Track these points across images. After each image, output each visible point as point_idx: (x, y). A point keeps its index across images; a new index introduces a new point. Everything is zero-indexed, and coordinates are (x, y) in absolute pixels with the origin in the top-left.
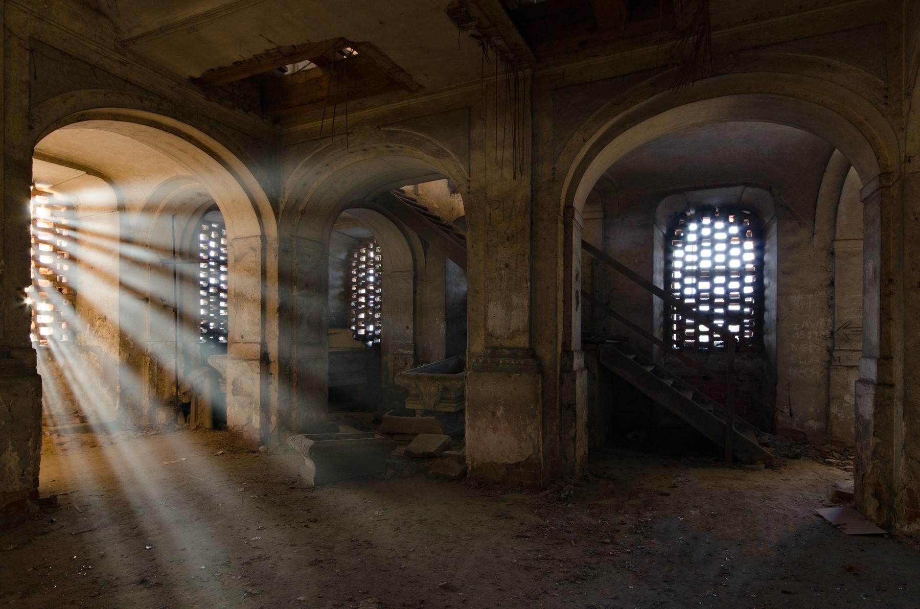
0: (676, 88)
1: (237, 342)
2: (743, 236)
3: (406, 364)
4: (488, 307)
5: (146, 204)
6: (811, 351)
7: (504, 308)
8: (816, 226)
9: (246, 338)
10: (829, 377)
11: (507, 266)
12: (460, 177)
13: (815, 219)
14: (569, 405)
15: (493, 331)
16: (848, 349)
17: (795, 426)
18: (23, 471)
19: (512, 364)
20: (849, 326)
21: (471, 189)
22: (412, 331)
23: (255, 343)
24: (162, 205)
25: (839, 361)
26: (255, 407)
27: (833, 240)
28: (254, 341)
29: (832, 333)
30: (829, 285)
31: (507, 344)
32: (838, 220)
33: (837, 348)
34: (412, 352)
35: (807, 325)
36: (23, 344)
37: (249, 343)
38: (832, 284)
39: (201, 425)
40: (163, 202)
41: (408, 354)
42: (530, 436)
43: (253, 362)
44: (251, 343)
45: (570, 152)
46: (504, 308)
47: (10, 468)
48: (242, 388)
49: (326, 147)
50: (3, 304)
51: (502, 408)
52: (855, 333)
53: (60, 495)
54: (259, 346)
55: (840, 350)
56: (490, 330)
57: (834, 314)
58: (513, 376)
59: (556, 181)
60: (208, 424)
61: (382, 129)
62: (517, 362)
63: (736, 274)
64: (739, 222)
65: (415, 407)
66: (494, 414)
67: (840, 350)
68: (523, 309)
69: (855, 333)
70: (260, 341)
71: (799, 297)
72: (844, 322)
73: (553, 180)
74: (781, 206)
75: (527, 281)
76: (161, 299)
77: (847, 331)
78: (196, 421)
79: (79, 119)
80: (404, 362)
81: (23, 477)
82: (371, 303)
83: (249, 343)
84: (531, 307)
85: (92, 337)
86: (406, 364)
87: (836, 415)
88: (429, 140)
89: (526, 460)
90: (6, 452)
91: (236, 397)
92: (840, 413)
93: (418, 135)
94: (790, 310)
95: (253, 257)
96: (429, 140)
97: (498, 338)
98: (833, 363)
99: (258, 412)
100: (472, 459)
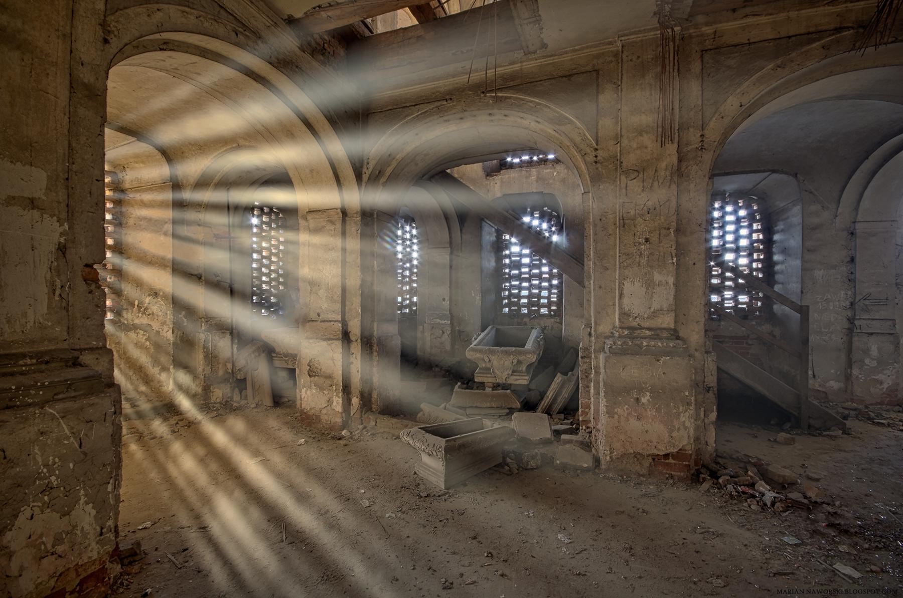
0: (863, 50)
1: (313, 321)
2: (751, 218)
3: (443, 333)
4: (623, 284)
5: (202, 176)
6: (832, 319)
7: (644, 285)
8: (839, 208)
9: (323, 316)
10: (850, 342)
11: (647, 240)
12: (586, 145)
13: (839, 203)
14: (710, 387)
15: (629, 310)
16: (867, 317)
17: (817, 386)
18: (102, 529)
19: (659, 347)
20: (869, 298)
21: (599, 158)
22: (448, 302)
23: (335, 321)
24: (217, 178)
25: (860, 329)
26: (336, 390)
27: (854, 222)
28: (334, 320)
29: (852, 304)
30: (849, 261)
31: (646, 324)
32: (861, 203)
33: (857, 317)
34: (449, 322)
35: (829, 297)
36: (95, 343)
37: (327, 321)
38: (852, 260)
39: (260, 403)
40: (218, 175)
41: (445, 324)
42: (684, 425)
43: (334, 341)
44: (331, 321)
45: (722, 118)
46: (644, 285)
47: (83, 528)
48: (321, 370)
49: (419, 115)
50: (67, 289)
51: (648, 394)
52: (873, 304)
53: (139, 529)
54: (340, 325)
55: (860, 319)
56: (626, 309)
57: (855, 287)
58: (662, 359)
59: (705, 149)
60: (268, 402)
61: (488, 95)
62: (665, 344)
63: (745, 251)
64: (747, 206)
65: (485, 380)
66: (638, 400)
67: (860, 319)
68: (668, 287)
69: (873, 304)
70: (340, 319)
71: (822, 271)
72: (864, 294)
73: (702, 148)
74: (806, 191)
75: (672, 257)
76: (215, 275)
77: (867, 302)
78: (254, 398)
79: (161, 47)
80: (441, 332)
81: (102, 537)
82: (400, 277)
83: (327, 321)
84: (676, 285)
85: (140, 315)
86: (443, 333)
87: (857, 377)
88: (546, 106)
89: (679, 450)
90: (77, 506)
91: (312, 378)
92: (861, 374)
93: (533, 101)
94: (814, 283)
95: (331, 230)
96: (546, 106)
97: (636, 317)
98: (855, 330)
99: (340, 395)
100: (610, 449)
